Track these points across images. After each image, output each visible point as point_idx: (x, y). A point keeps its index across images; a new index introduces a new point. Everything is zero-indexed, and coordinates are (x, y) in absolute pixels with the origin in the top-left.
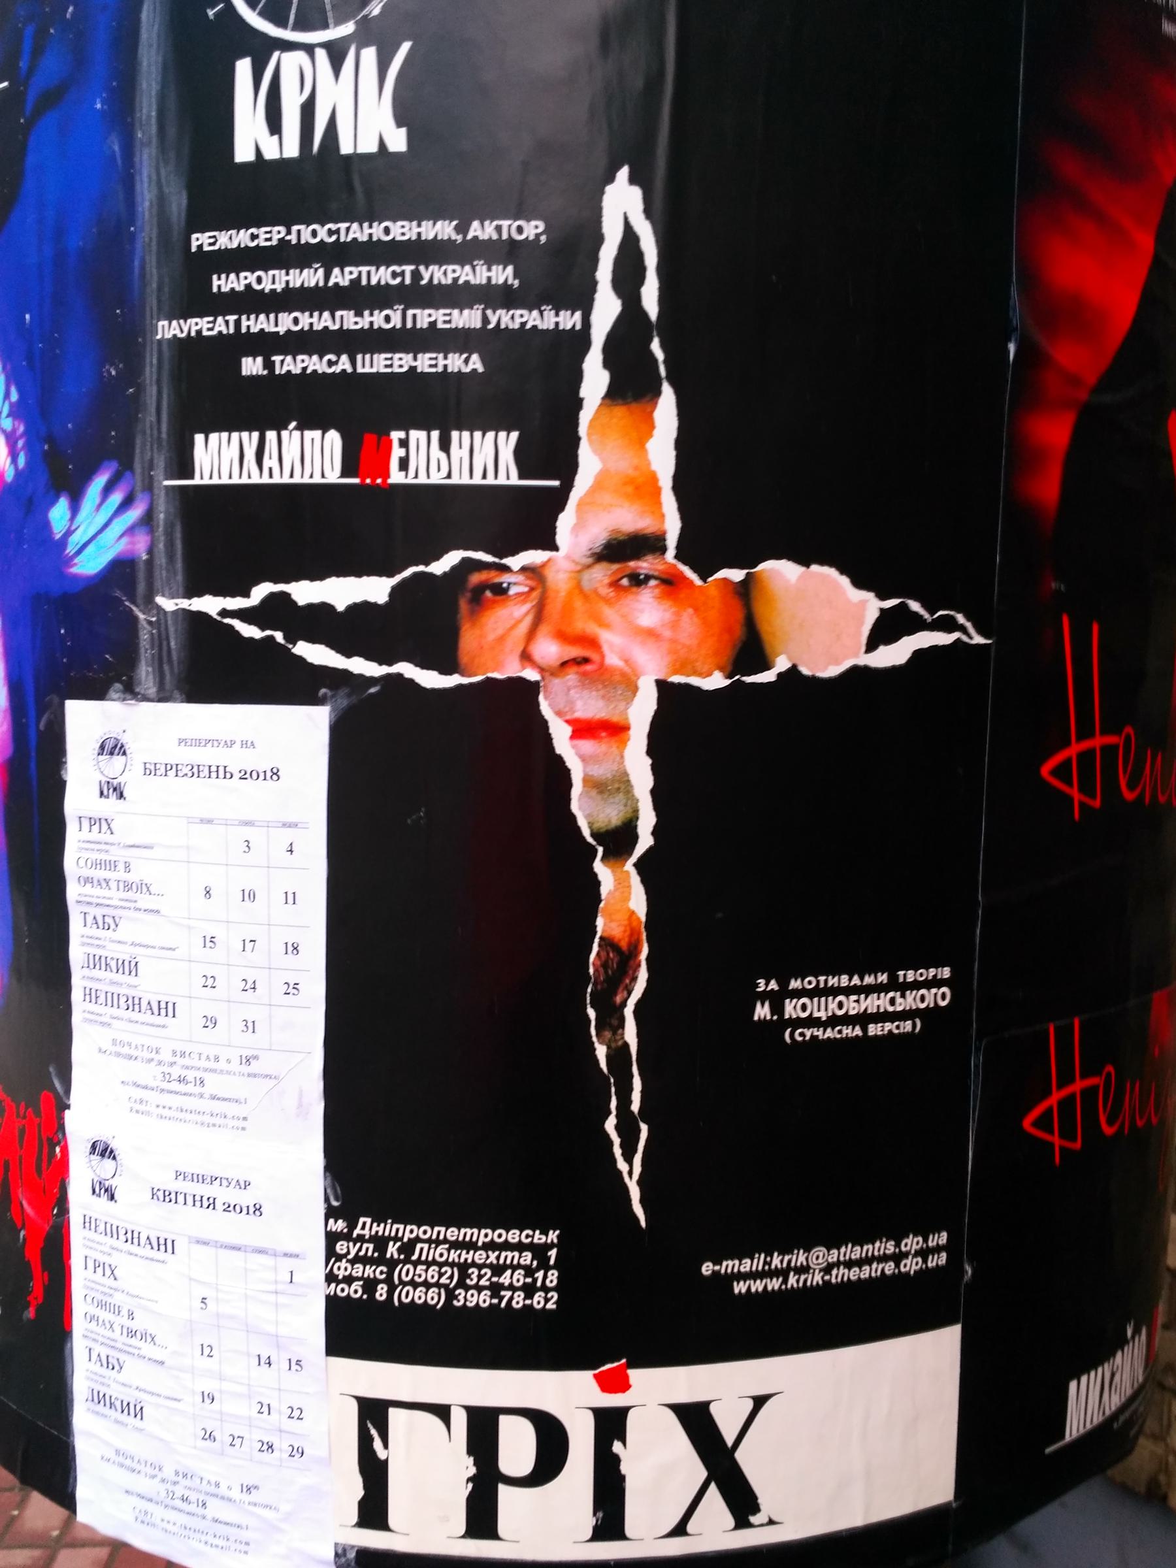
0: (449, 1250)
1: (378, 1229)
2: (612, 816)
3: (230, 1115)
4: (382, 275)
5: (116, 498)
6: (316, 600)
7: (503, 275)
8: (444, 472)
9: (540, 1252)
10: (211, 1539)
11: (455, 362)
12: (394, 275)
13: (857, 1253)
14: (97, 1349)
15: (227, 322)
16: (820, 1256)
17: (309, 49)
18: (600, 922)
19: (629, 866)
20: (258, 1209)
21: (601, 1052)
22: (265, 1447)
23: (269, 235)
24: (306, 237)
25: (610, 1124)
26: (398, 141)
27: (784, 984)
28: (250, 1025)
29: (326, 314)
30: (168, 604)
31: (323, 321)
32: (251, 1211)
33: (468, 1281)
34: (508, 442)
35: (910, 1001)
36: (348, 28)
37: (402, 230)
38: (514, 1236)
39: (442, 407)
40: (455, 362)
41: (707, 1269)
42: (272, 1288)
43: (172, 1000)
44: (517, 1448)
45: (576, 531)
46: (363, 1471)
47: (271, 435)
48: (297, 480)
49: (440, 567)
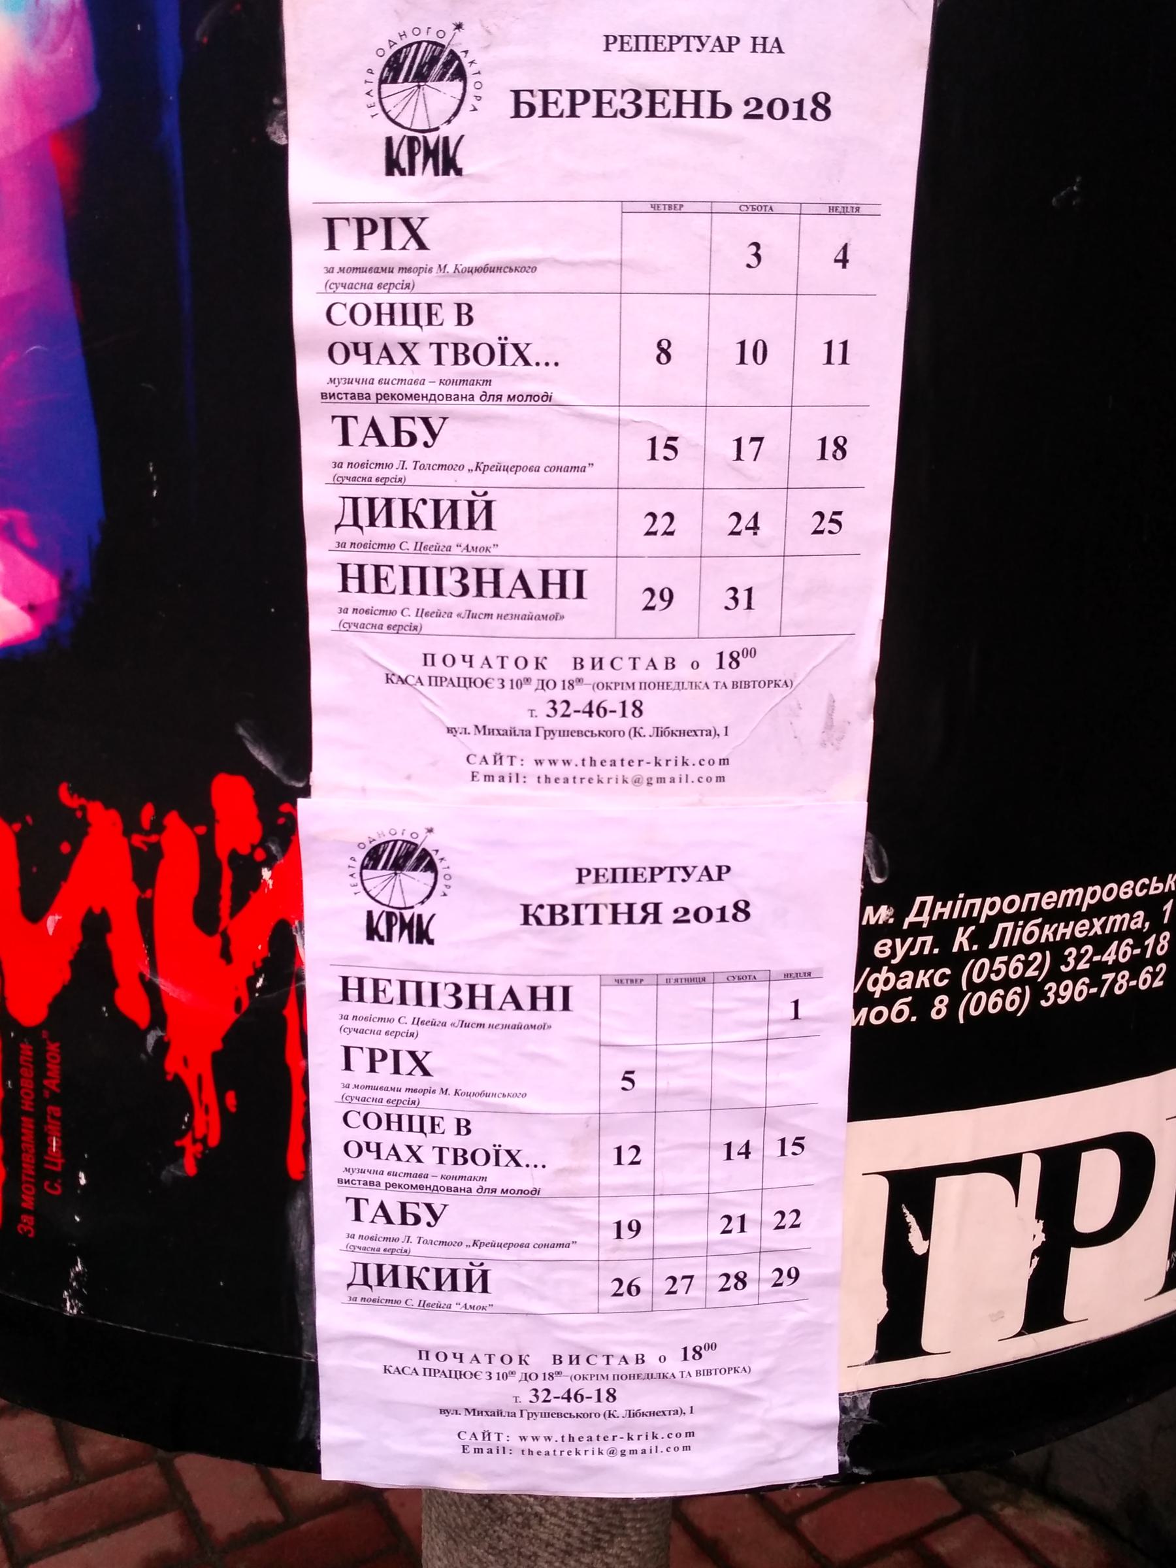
0: (1041, 927)
1: (944, 910)
3: (693, 758)
20: (742, 910)
22: (733, 1281)
28: (742, 596)
32: (729, 916)
33: (1063, 968)
38: (1127, 890)
42: (761, 1032)
43: (572, 565)
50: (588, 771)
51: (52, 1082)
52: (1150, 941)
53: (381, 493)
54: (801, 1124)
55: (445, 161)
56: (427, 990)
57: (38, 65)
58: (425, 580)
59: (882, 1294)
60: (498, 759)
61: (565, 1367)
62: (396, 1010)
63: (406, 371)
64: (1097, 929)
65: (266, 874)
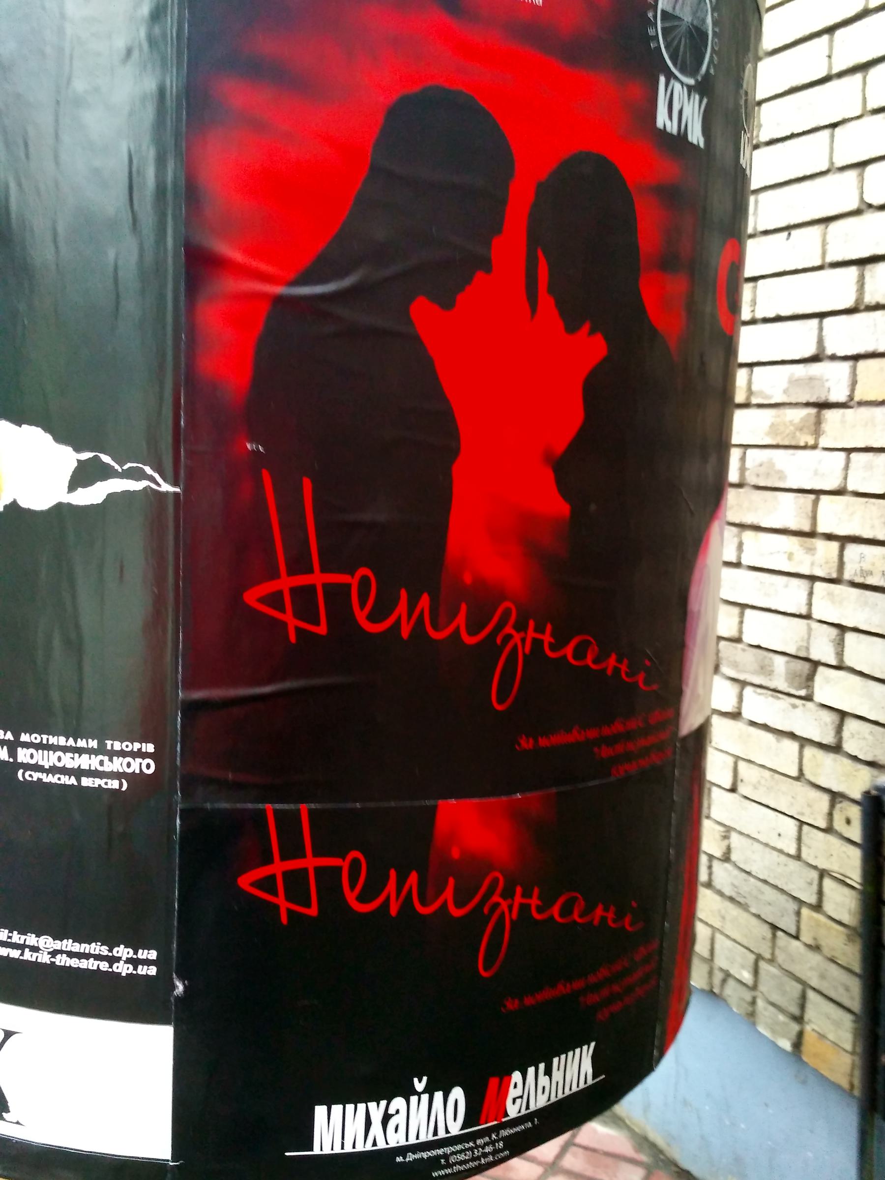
13: (77, 947)
16: (47, 942)
27: (17, 736)
35: (117, 765)
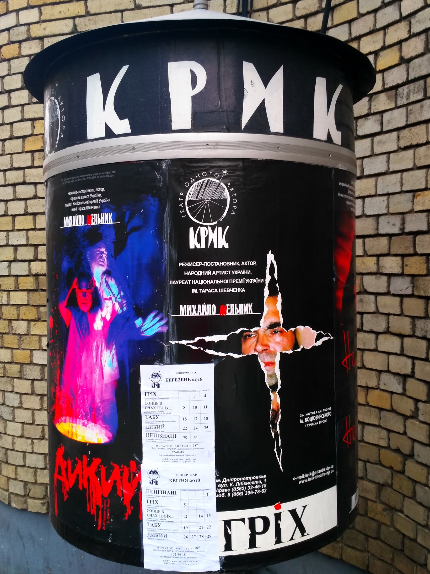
1: (228, 480)
2: (273, 382)
4: (224, 273)
5: (157, 319)
6: (211, 340)
7: (249, 272)
8: (238, 312)
9: (262, 480)
10: (187, 563)
11: (240, 290)
12: (226, 273)
14: (151, 522)
15: (188, 282)
16: (314, 473)
17: (207, 227)
18: (271, 406)
19: (277, 393)
20: (199, 480)
21: (273, 434)
23: (198, 264)
24: (207, 264)
25: (275, 450)
26: (227, 246)
27: (305, 415)
29: (212, 280)
30: (173, 343)
31: (211, 282)
34: (250, 305)
36: (215, 223)
37: (228, 264)
38: (257, 477)
39: (239, 299)
40: (240, 290)
41: (294, 479)
42: (203, 498)
44: (259, 525)
45: (264, 323)
46: (225, 538)
47: (199, 306)
48: (206, 315)
49: (237, 332)
50: (177, 461)
51: (108, 506)
52: (263, 485)
53: (151, 424)
54: (210, 512)
55: (158, 386)
56: (157, 491)
57: (113, 373)
58: (156, 435)
59: (225, 540)
60: (166, 459)
61: (178, 550)
62: (153, 494)
63: (154, 410)
64: (253, 483)
65: (137, 475)
